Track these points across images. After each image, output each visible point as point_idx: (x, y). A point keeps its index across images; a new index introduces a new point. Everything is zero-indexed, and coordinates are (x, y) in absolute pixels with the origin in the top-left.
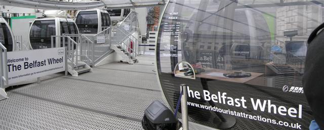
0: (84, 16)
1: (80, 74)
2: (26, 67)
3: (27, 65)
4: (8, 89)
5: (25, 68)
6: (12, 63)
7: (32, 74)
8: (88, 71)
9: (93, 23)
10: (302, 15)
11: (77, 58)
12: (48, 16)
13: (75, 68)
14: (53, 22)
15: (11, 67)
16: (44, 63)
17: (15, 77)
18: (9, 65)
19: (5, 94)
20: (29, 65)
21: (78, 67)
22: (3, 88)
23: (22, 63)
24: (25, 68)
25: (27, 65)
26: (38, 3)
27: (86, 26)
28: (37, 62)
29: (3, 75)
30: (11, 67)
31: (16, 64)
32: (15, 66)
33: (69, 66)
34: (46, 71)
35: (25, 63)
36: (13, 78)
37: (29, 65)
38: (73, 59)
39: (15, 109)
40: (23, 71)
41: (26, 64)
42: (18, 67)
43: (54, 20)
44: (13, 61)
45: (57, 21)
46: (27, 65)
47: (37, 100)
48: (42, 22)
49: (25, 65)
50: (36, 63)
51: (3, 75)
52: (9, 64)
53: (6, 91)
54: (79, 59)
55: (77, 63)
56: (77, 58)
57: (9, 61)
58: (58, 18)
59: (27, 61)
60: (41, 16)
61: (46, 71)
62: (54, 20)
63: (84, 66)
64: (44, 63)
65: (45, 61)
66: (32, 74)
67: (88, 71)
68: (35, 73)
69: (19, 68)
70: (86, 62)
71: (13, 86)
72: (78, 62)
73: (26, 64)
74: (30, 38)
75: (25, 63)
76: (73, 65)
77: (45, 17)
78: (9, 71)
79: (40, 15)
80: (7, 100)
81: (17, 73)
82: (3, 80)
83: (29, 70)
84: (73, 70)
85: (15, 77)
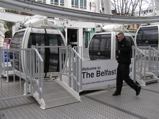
0: (146, 32)
1: (147, 84)
2: (98, 75)
3: (99, 73)
4: (81, 94)
5: (97, 76)
6: (86, 71)
7: (103, 81)
8: (156, 82)
9: (153, 38)
10: (40, 40)
11: (145, 68)
12: (106, 30)
13: (143, 78)
14: (108, 38)
15: (85, 74)
16: (114, 72)
17: (88, 84)
18: (84, 73)
19: (78, 98)
20: (100, 73)
21: (146, 77)
22: (78, 92)
23: (95, 72)
24: (97, 76)
25: (99, 73)
26: (92, 17)
27: (147, 42)
28: (108, 71)
29: (78, 81)
30: (85, 74)
31: (90, 72)
32: (89, 74)
33: (137, 76)
34: (93, 83)
35: (97, 71)
36: (86, 84)
37: (100, 73)
38: (141, 69)
39: (85, 112)
40: (95, 79)
41: (98, 72)
42: (91, 75)
43: (111, 34)
44: (87, 69)
45: (113, 35)
46: (99, 74)
47: (103, 105)
48: (102, 36)
49: (97, 74)
50: (107, 72)
51: (78, 81)
52: (83, 71)
53: (80, 95)
54: (147, 69)
55: (145, 73)
56: (145, 68)
57: (83, 69)
58: (115, 33)
59: (99, 70)
60: (100, 31)
61: (93, 83)
62: (111, 34)
63: (152, 77)
64: (114, 72)
65: (115, 70)
66: (103, 81)
67: (156, 82)
68: (106, 81)
69: (92, 75)
70: (154, 73)
71: (91, 91)
72: (147, 73)
73: (98, 72)
74: (116, 51)
75: (97, 71)
76: (142, 75)
77: (104, 31)
78: (84, 78)
79: (99, 29)
80: (79, 103)
81: (90, 80)
82: (78, 86)
83: (101, 78)
84: (140, 79)
85: (88, 84)
